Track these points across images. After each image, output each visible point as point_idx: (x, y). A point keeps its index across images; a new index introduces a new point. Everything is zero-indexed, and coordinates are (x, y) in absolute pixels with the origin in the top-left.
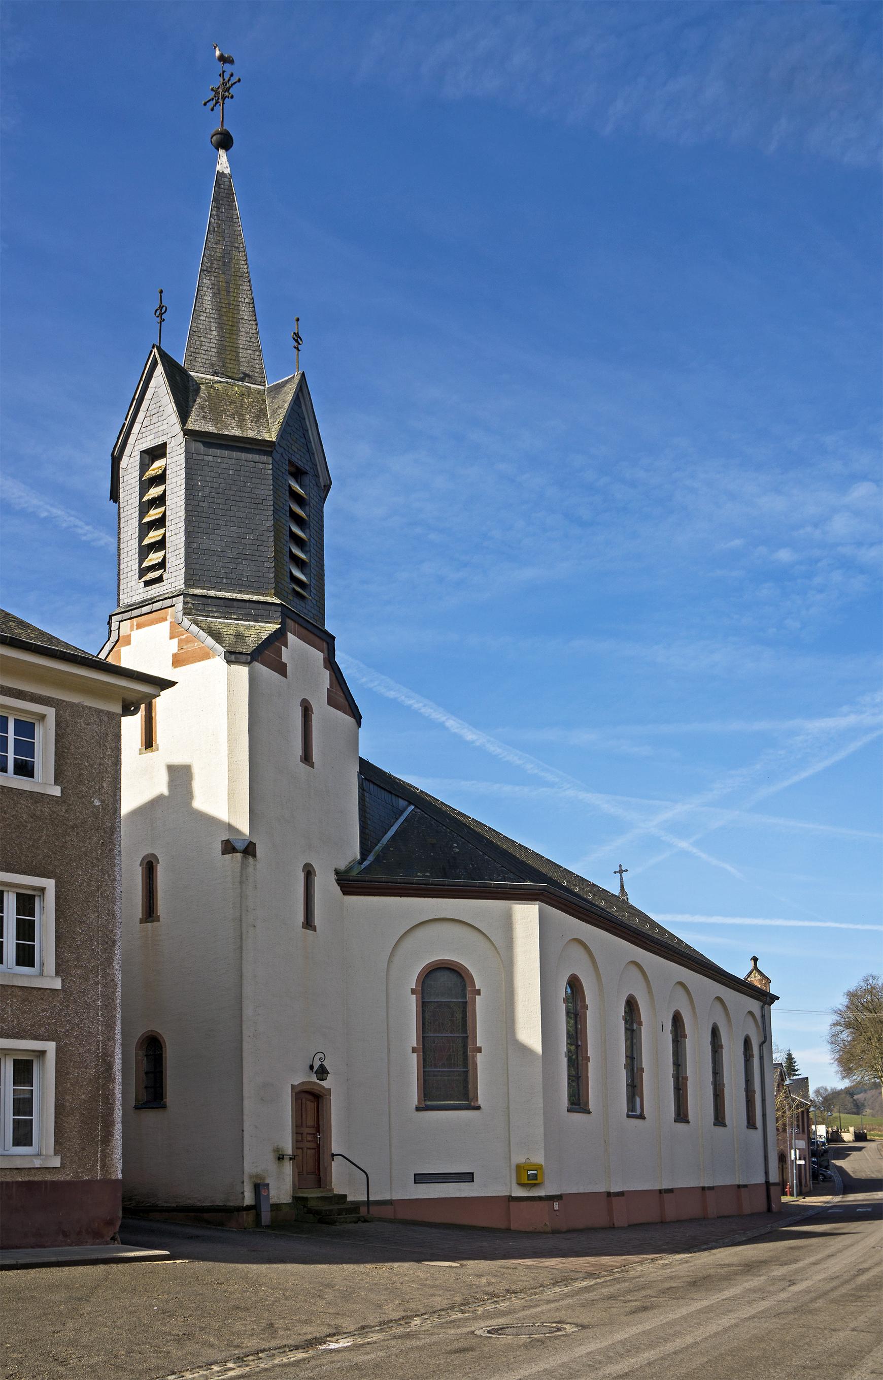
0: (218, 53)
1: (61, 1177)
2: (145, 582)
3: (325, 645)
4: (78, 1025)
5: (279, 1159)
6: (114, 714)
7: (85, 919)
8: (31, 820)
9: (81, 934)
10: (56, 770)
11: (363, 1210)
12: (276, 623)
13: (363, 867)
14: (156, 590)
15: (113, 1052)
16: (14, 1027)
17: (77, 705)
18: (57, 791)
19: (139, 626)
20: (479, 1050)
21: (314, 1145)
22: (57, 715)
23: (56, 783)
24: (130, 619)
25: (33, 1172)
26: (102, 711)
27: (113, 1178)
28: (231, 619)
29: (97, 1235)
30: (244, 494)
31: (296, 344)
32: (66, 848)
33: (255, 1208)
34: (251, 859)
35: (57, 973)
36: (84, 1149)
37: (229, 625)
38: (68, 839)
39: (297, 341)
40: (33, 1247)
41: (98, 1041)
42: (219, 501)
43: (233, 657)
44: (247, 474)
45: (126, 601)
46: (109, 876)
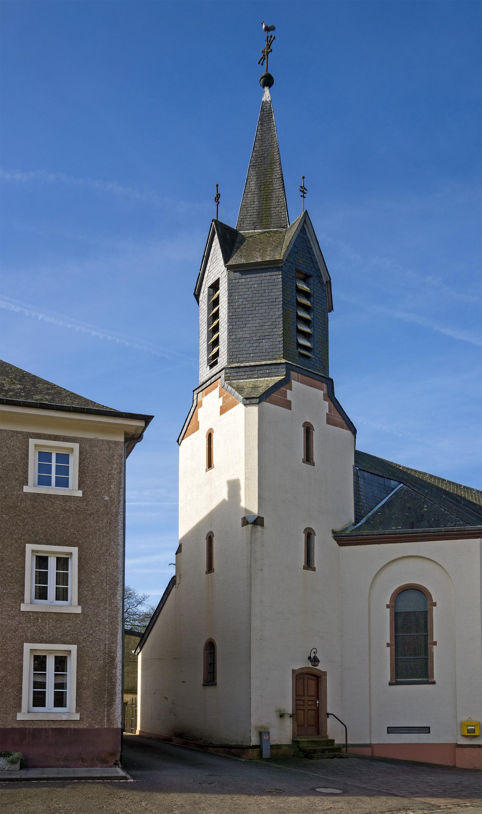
0: (264, 26)
1: (81, 726)
2: (210, 366)
3: (325, 385)
4: (92, 635)
5: (281, 716)
6: (118, 442)
7: (98, 570)
8: (63, 512)
9: (95, 579)
10: (79, 481)
11: (344, 749)
12: (282, 376)
13: (356, 527)
14: (216, 369)
15: (116, 651)
16: (50, 637)
17: (94, 440)
18: (80, 494)
19: (206, 394)
20: (435, 643)
21: (314, 708)
22: (80, 447)
23: (79, 488)
24: (202, 391)
25: (63, 722)
26: (111, 441)
27: (115, 727)
28: (254, 378)
29: (104, 762)
30: (264, 298)
31: (302, 194)
32: (86, 528)
33: (259, 747)
34: (259, 528)
35: (79, 604)
36: (95, 709)
37: (247, 383)
38: (87, 522)
39: (303, 192)
40: (62, 767)
41: (106, 644)
42: (248, 306)
43: (248, 401)
44: (266, 285)
45: (202, 380)
46: (115, 543)
